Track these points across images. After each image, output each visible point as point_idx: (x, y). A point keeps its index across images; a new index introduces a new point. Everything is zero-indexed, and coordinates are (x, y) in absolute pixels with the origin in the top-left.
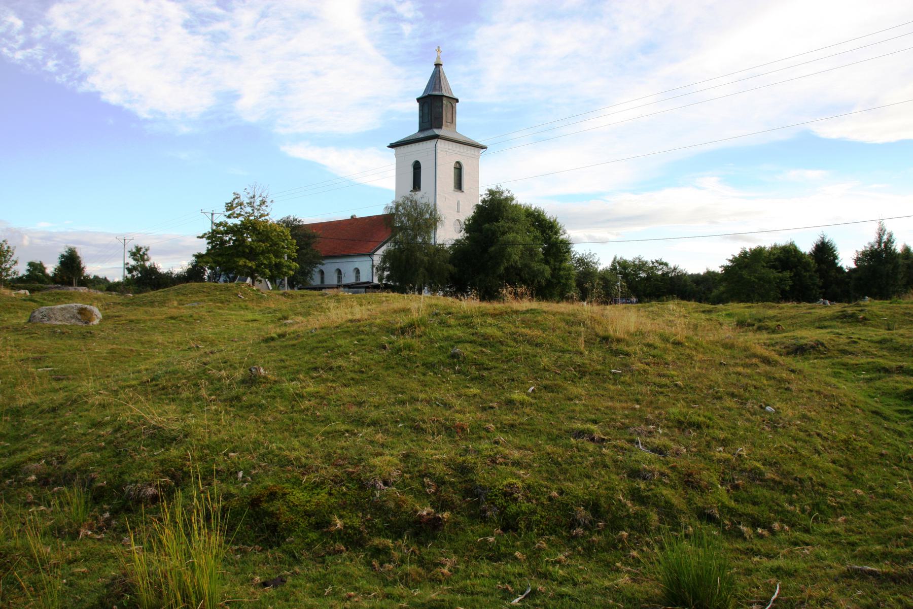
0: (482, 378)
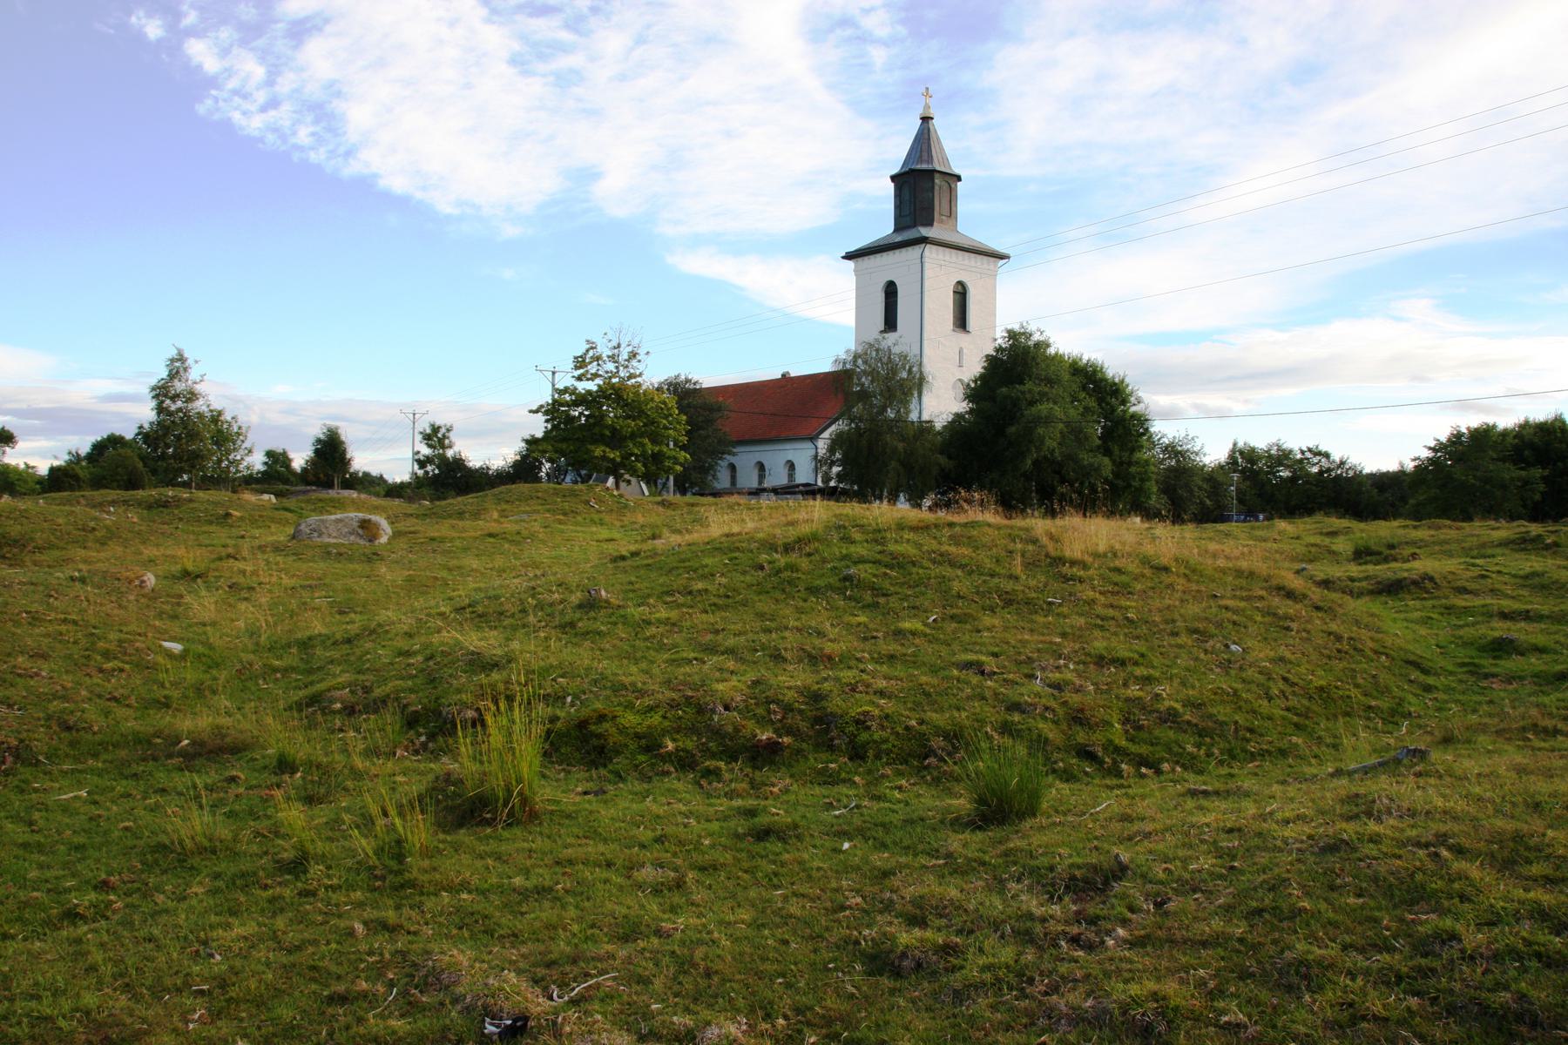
0: (876, 605)
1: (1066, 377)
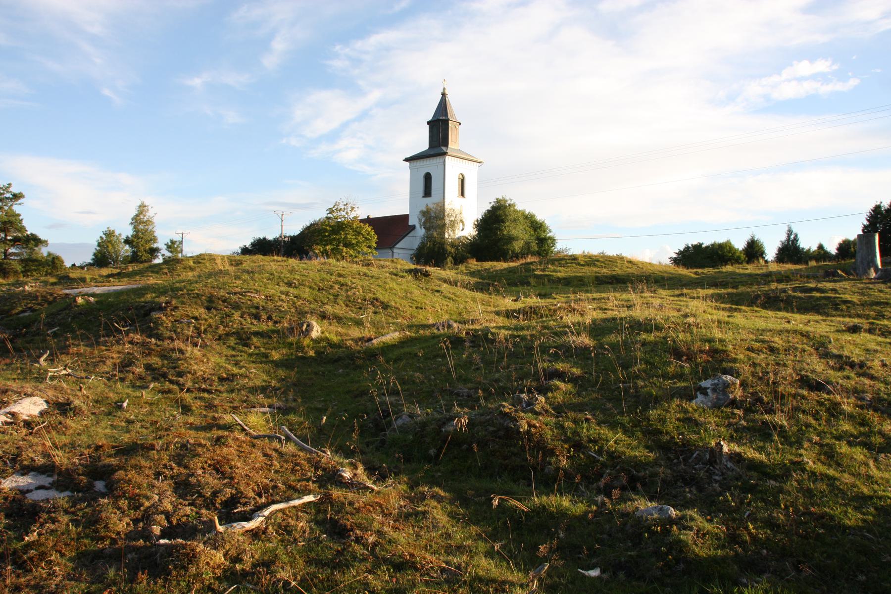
1: (521, 219)
